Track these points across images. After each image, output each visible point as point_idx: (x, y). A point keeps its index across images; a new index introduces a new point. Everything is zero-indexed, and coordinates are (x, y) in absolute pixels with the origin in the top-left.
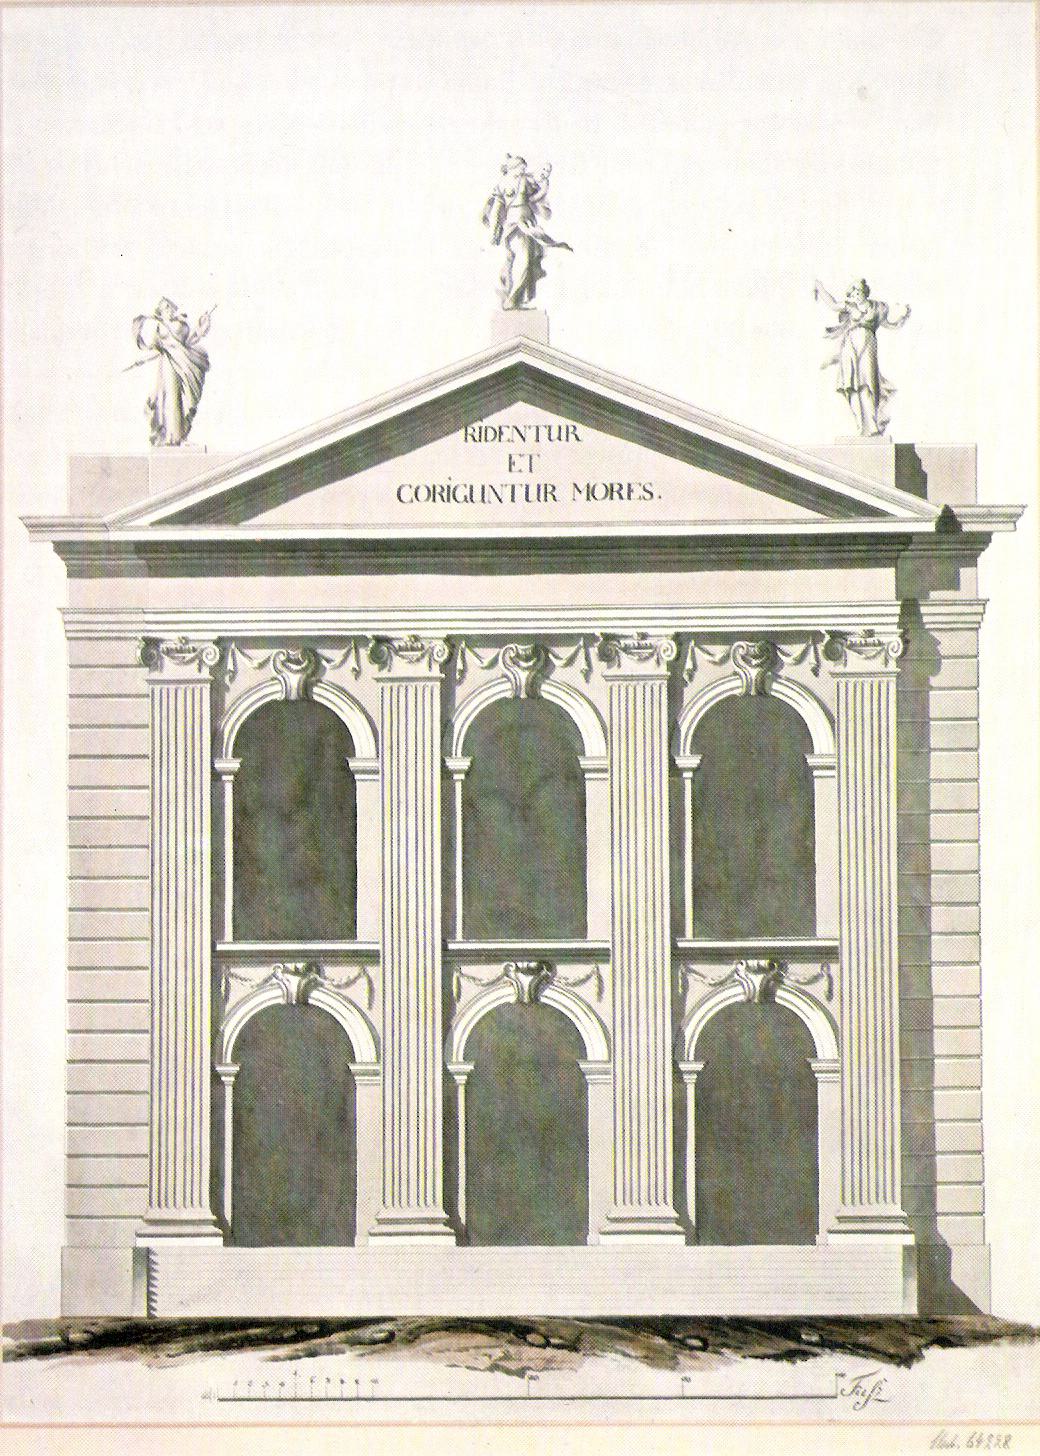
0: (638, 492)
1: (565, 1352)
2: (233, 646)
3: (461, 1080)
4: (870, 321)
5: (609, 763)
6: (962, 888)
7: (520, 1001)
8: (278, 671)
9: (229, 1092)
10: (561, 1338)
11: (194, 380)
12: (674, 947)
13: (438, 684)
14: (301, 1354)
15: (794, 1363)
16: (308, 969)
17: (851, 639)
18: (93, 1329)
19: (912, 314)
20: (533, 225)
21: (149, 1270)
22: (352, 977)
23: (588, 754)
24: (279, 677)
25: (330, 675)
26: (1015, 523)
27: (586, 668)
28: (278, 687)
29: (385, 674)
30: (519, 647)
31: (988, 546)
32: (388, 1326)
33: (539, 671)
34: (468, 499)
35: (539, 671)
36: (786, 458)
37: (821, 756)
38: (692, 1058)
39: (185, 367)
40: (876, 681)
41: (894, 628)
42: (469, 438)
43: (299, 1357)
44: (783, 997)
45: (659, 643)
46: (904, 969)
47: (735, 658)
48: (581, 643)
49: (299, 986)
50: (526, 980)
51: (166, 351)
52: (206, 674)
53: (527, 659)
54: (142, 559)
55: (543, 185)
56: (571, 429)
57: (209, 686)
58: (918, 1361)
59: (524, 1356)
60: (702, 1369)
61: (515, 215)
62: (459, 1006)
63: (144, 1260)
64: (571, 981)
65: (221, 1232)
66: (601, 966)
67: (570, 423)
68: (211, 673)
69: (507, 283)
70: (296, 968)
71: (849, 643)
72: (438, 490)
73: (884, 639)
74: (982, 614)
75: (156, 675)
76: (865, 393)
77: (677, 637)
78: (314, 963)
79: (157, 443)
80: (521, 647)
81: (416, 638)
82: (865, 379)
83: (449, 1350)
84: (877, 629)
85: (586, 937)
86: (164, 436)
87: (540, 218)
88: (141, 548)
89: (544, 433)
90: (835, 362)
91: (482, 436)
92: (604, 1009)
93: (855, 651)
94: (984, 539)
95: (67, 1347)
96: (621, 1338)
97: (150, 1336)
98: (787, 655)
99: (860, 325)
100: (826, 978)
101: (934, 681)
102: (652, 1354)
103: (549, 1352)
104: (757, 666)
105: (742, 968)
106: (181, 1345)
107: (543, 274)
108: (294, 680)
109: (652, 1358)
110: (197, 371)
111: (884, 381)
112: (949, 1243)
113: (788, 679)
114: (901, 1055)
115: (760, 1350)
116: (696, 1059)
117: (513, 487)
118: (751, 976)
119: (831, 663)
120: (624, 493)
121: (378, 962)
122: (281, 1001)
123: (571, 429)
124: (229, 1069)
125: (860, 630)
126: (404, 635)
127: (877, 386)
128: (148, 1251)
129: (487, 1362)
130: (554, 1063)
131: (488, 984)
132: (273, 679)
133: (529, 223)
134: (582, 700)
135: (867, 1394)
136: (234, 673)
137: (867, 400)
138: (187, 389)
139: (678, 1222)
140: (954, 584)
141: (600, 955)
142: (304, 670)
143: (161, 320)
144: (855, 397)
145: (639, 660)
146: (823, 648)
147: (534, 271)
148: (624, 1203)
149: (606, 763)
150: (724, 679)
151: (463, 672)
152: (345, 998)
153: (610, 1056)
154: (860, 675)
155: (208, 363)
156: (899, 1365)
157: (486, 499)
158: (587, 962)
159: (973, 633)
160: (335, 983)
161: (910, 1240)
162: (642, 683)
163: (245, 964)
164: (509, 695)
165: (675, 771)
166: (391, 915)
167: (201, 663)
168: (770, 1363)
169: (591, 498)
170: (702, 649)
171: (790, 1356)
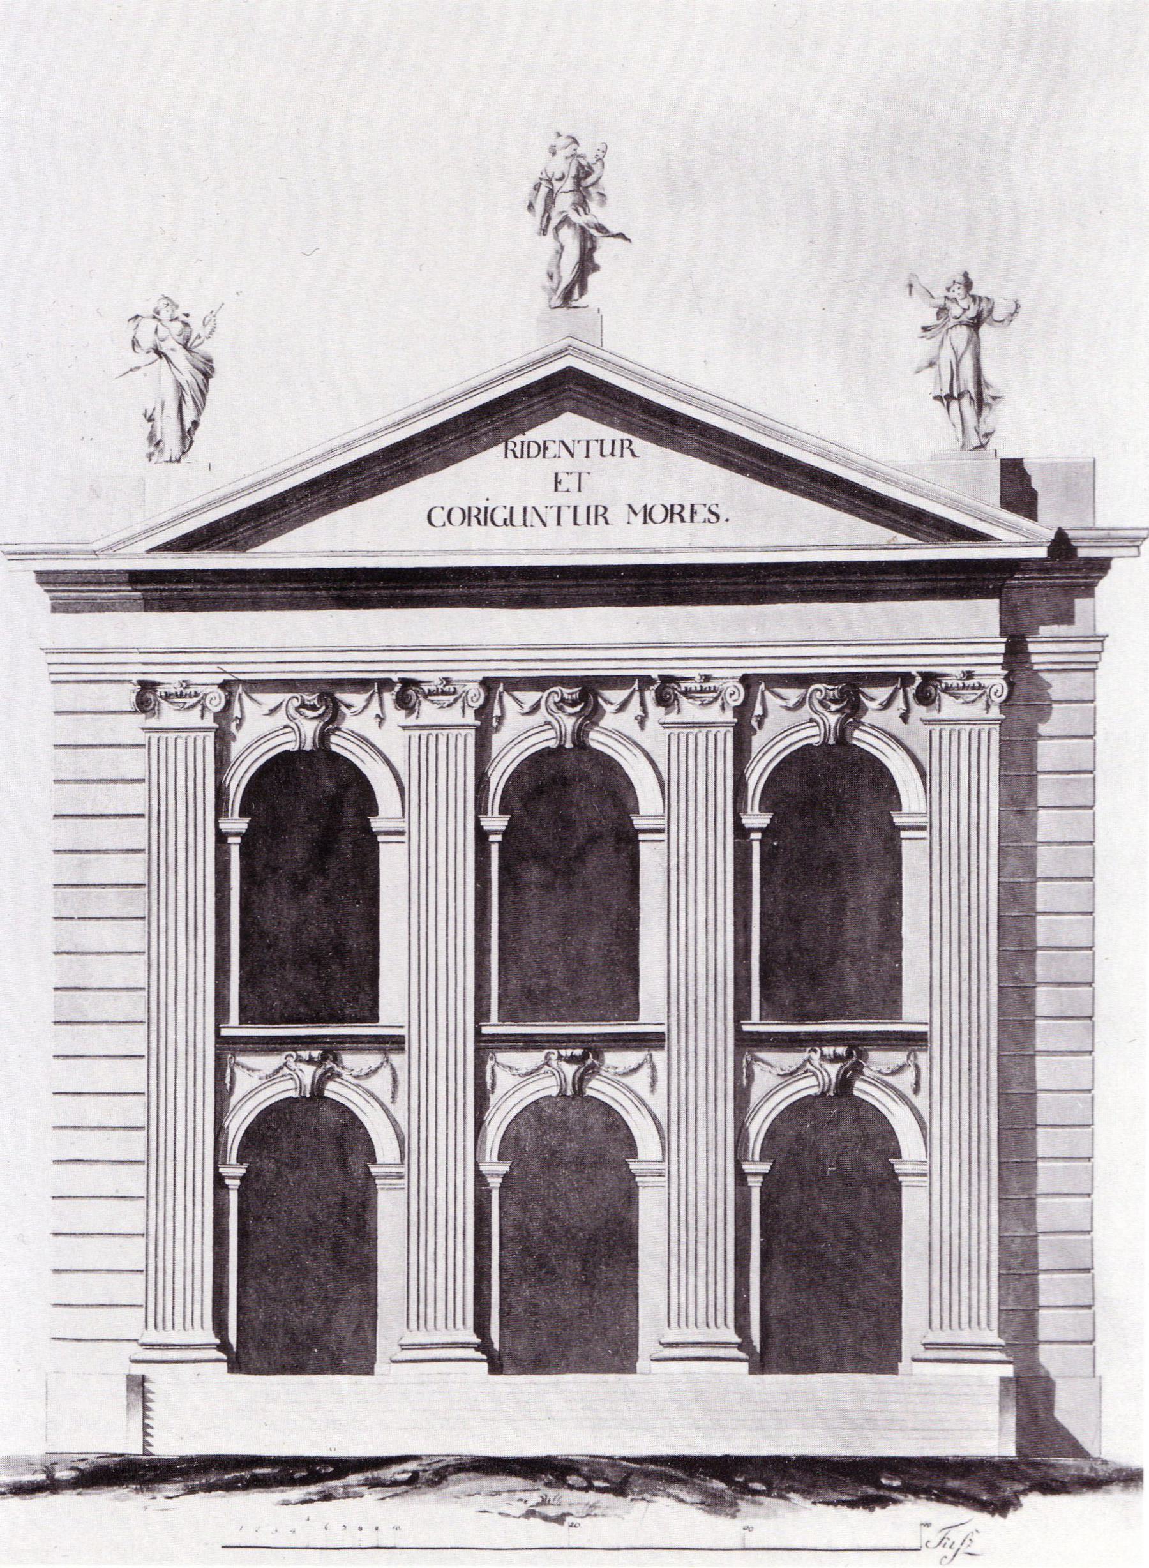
0: (702, 513)
1: (611, 1496)
2: (240, 690)
3: (495, 1183)
4: (972, 319)
5: (928, 820)
6: (1071, 969)
7: (562, 1094)
8: (292, 719)
9: (233, 1197)
10: (606, 1480)
11: (196, 388)
12: (738, 1030)
13: (473, 732)
14: (314, 1498)
15: (872, 1510)
16: (324, 1058)
17: (946, 681)
18: (82, 1466)
19: (1021, 311)
20: (586, 214)
21: (145, 1399)
22: (373, 1068)
23: (641, 813)
24: (292, 725)
25: (350, 723)
26: (1138, 546)
27: (641, 713)
28: (291, 737)
29: (412, 720)
30: (563, 690)
31: (1106, 573)
32: (412, 1466)
33: (587, 718)
34: (508, 522)
35: (587, 718)
36: (873, 475)
37: (910, 814)
38: (757, 1158)
39: (188, 375)
40: (976, 728)
41: (998, 670)
42: (510, 454)
43: (311, 1501)
44: (861, 1089)
45: (725, 686)
46: (1005, 1060)
47: (811, 704)
48: (636, 686)
49: (314, 1077)
50: (570, 1070)
51: (166, 356)
52: (209, 721)
53: (574, 704)
54: (137, 590)
55: (597, 168)
56: (626, 444)
57: (212, 735)
58: (1015, 1509)
59: (564, 1500)
60: (767, 1517)
61: (565, 202)
62: (493, 1099)
63: (138, 1386)
64: (621, 1070)
65: (225, 1357)
66: (655, 1053)
67: (626, 436)
68: (215, 721)
69: (555, 276)
70: (835, 1053)
71: (943, 685)
72: (474, 512)
73: (986, 682)
74: (1099, 653)
75: (153, 722)
76: (965, 401)
77: (745, 680)
78: (331, 1049)
79: (154, 459)
80: (566, 691)
81: (448, 681)
82: (966, 385)
83: (479, 1494)
84: (978, 670)
85: (637, 1019)
86: (161, 451)
87: (593, 205)
88: (136, 578)
89: (595, 448)
90: (931, 364)
91: (525, 452)
92: (658, 1102)
93: (951, 695)
94: (1101, 566)
95: (52, 1486)
96: (671, 1480)
97: (145, 1475)
98: (872, 699)
99: (961, 323)
100: (912, 1068)
101: (1043, 729)
102: (709, 1500)
103: (592, 1497)
104: (837, 711)
105: (816, 1057)
106: (180, 1486)
107: (596, 268)
108: (310, 728)
109: (714, 1503)
110: (200, 377)
111: (987, 385)
112: (1053, 1374)
113: (873, 727)
114: (999, 1157)
115: (836, 1496)
116: (763, 1158)
117: (559, 509)
118: (827, 1066)
119: (923, 709)
120: (686, 514)
121: (403, 1049)
122: (294, 1094)
123: (626, 444)
124: (234, 1171)
125: (956, 671)
126: (435, 678)
127: (980, 393)
128: (144, 1379)
129: (521, 1508)
130: (601, 1162)
131: (526, 1074)
132: (286, 727)
133: (581, 210)
134: (636, 751)
135: (956, 1546)
136: (241, 719)
137: (969, 409)
138: (188, 399)
139: (740, 1347)
140: (1067, 617)
141: (653, 1041)
142: (320, 716)
143: (160, 320)
144: (954, 405)
145: (702, 704)
146: (914, 691)
147: (586, 265)
148: (708, 1325)
149: (661, 823)
150: (796, 727)
151: (501, 719)
152: (366, 1091)
153: (663, 1155)
154: (956, 721)
155: (212, 368)
156: (992, 1513)
157: (528, 523)
158: (638, 1048)
159: (1089, 674)
160: (354, 1073)
161: (1008, 1371)
162: (704, 731)
163: (254, 1052)
164: (553, 744)
165: (741, 832)
166: (418, 997)
167: (204, 708)
168: (844, 1511)
169: (648, 520)
170: (251, 698)
171: (868, 1503)
